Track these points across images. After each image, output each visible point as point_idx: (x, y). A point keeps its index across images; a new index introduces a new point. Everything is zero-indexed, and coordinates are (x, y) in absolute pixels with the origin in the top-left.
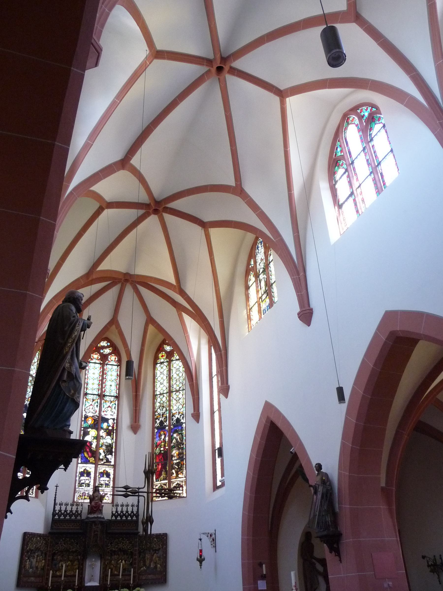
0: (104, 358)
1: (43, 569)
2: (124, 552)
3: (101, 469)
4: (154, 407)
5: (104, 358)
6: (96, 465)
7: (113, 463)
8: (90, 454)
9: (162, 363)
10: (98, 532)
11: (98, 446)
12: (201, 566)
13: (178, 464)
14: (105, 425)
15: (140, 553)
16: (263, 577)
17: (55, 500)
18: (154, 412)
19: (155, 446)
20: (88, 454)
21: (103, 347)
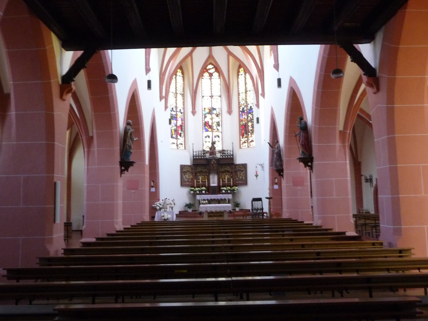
0: (211, 75)
1: (192, 179)
2: (228, 172)
3: (215, 134)
4: (239, 100)
5: (211, 75)
6: (212, 132)
7: (220, 131)
8: (208, 127)
9: (241, 75)
10: (275, 149)
11: (212, 123)
12: (257, 178)
13: (251, 130)
14: (214, 112)
15: (235, 172)
16: (276, 184)
17: (193, 150)
18: (239, 103)
19: (240, 121)
20: (208, 127)
21: (210, 69)
